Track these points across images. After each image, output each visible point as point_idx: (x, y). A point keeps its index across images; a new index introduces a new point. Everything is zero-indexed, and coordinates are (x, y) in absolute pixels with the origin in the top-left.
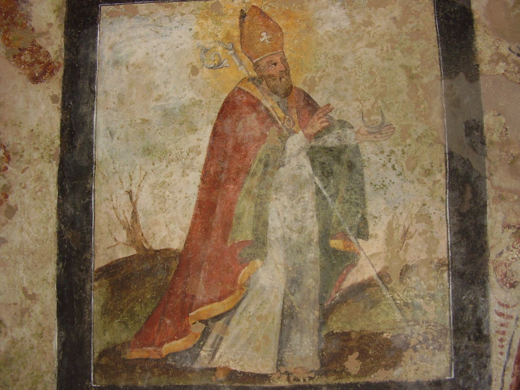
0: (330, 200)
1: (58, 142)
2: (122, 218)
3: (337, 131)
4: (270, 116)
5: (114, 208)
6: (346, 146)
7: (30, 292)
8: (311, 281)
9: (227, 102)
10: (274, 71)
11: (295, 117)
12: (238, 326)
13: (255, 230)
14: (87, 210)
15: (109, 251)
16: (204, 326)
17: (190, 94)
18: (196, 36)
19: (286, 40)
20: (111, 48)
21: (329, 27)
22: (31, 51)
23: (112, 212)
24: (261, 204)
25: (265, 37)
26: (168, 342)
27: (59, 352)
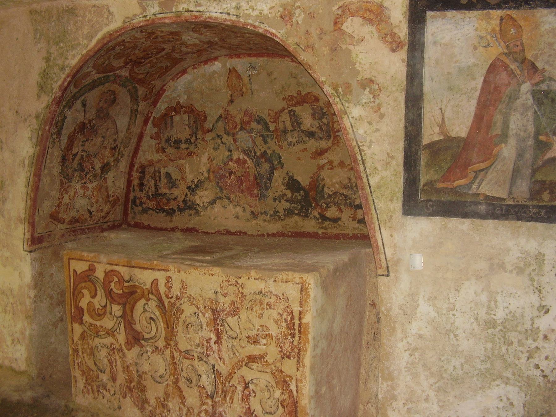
0: (541, 117)
1: (405, 83)
2: (437, 121)
3: (547, 82)
4: (513, 73)
5: (433, 116)
6: (551, 90)
7: (390, 155)
8: (528, 156)
9: (491, 65)
10: (517, 49)
11: (526, 74)
12: (492, 175)
13: (502, 130)
14: (420, 116)
15: (430, 137)
16: (475, 174)
17: (472, 61)
18: (477, 29)
19: (524, 33)
20: (432, 35)
21: (547, 27)
22: (391, 35)
23: (432, 118)
24: (506, 117)
25: (513, 31)
26: (457, 180)
27: (404, 183)
